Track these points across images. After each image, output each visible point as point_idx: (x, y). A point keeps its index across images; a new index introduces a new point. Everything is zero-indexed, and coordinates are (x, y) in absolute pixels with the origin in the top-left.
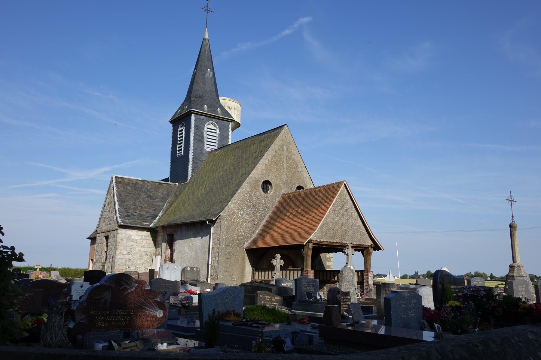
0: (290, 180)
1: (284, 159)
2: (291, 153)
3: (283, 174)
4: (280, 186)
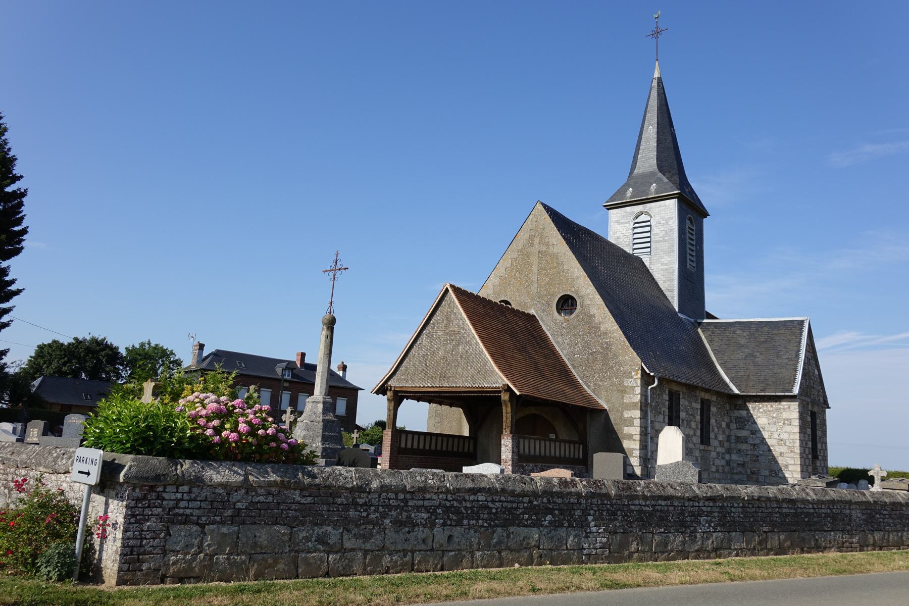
0: (547, 290)
1: (535, 260)
2: (548, 244)
3: (532, 283)
4: (525, 303)
